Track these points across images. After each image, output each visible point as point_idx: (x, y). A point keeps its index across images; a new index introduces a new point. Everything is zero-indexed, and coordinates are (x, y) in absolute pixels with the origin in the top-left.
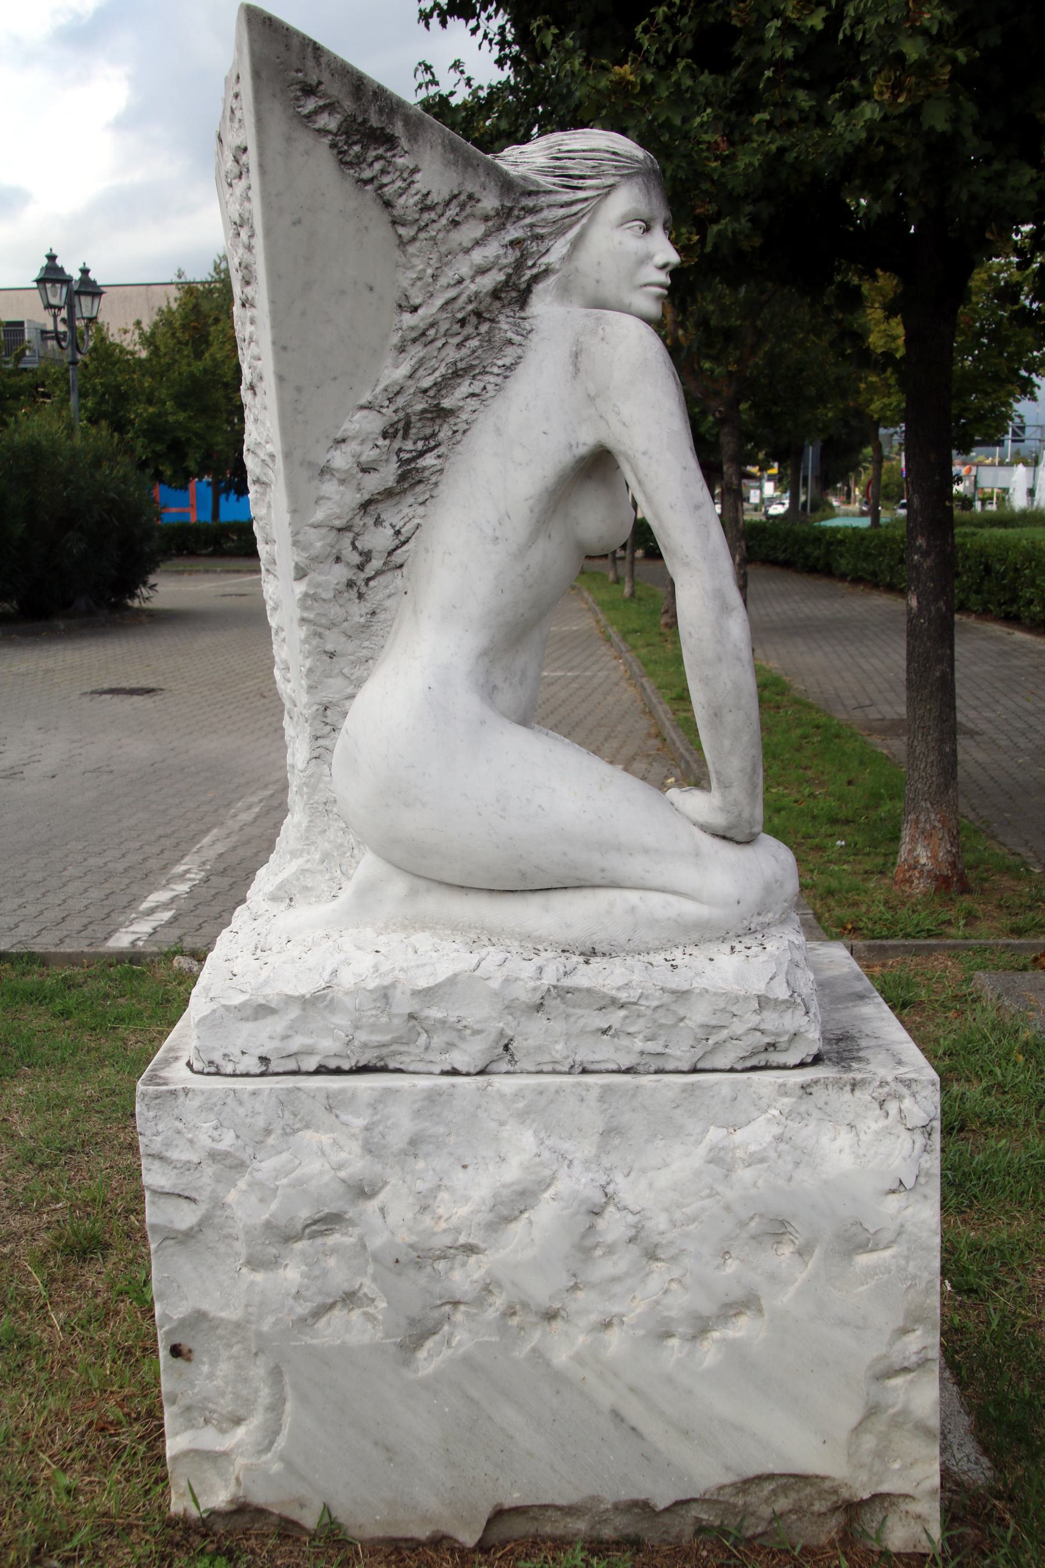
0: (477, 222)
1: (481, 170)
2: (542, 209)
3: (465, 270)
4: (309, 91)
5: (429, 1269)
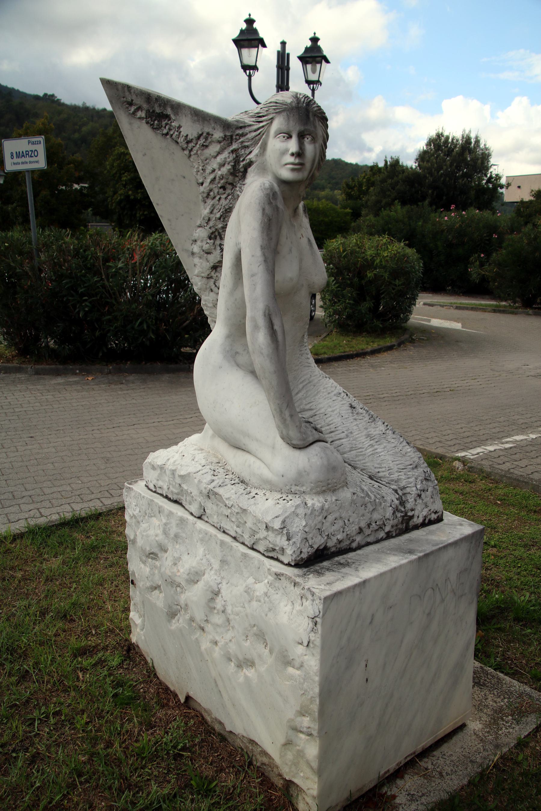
0: (216, 144)
1: (212, 122)
2: (247, 134)
3: (215, 166)
4: (131, 104)
5: (175, 588)
